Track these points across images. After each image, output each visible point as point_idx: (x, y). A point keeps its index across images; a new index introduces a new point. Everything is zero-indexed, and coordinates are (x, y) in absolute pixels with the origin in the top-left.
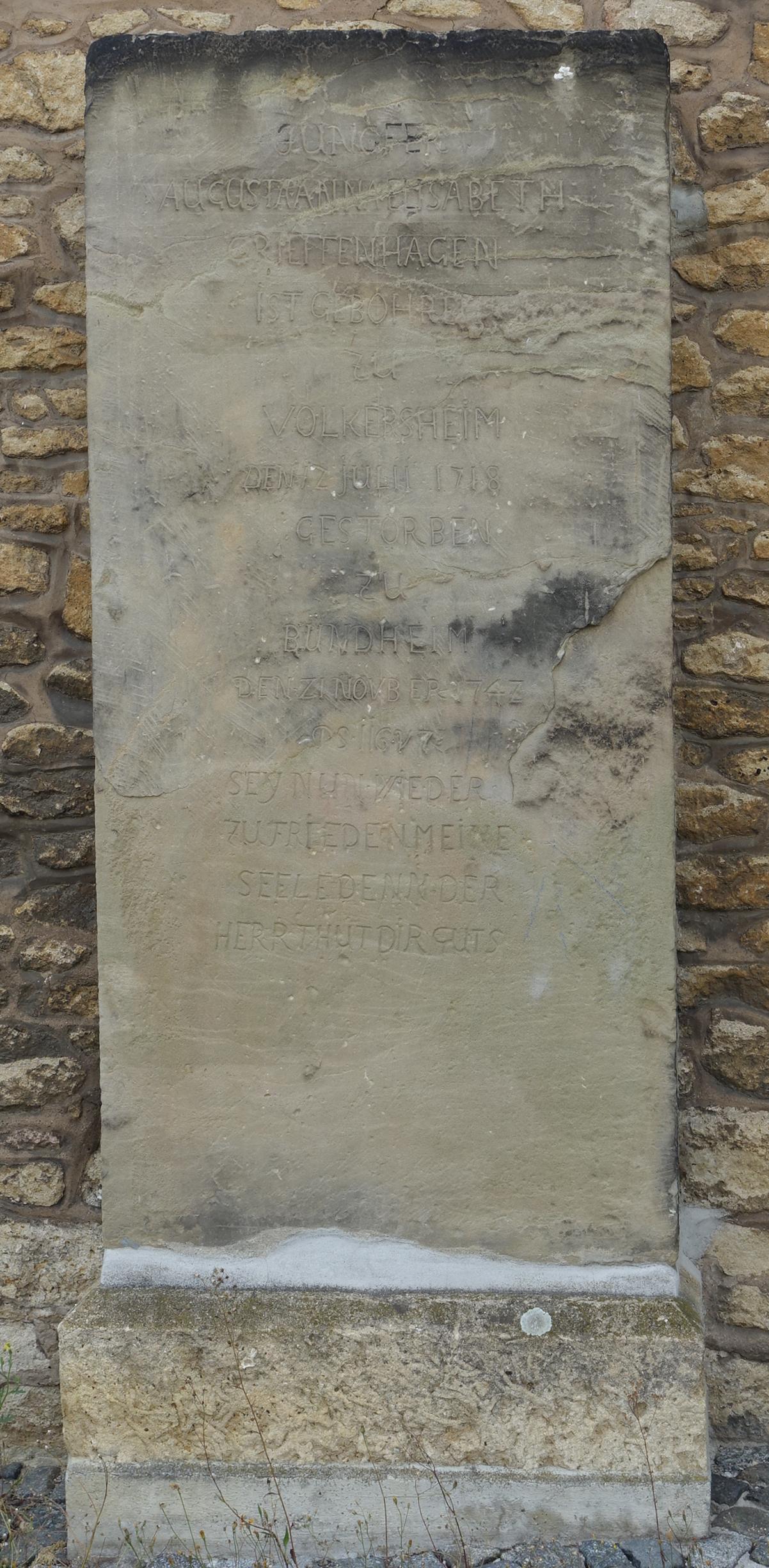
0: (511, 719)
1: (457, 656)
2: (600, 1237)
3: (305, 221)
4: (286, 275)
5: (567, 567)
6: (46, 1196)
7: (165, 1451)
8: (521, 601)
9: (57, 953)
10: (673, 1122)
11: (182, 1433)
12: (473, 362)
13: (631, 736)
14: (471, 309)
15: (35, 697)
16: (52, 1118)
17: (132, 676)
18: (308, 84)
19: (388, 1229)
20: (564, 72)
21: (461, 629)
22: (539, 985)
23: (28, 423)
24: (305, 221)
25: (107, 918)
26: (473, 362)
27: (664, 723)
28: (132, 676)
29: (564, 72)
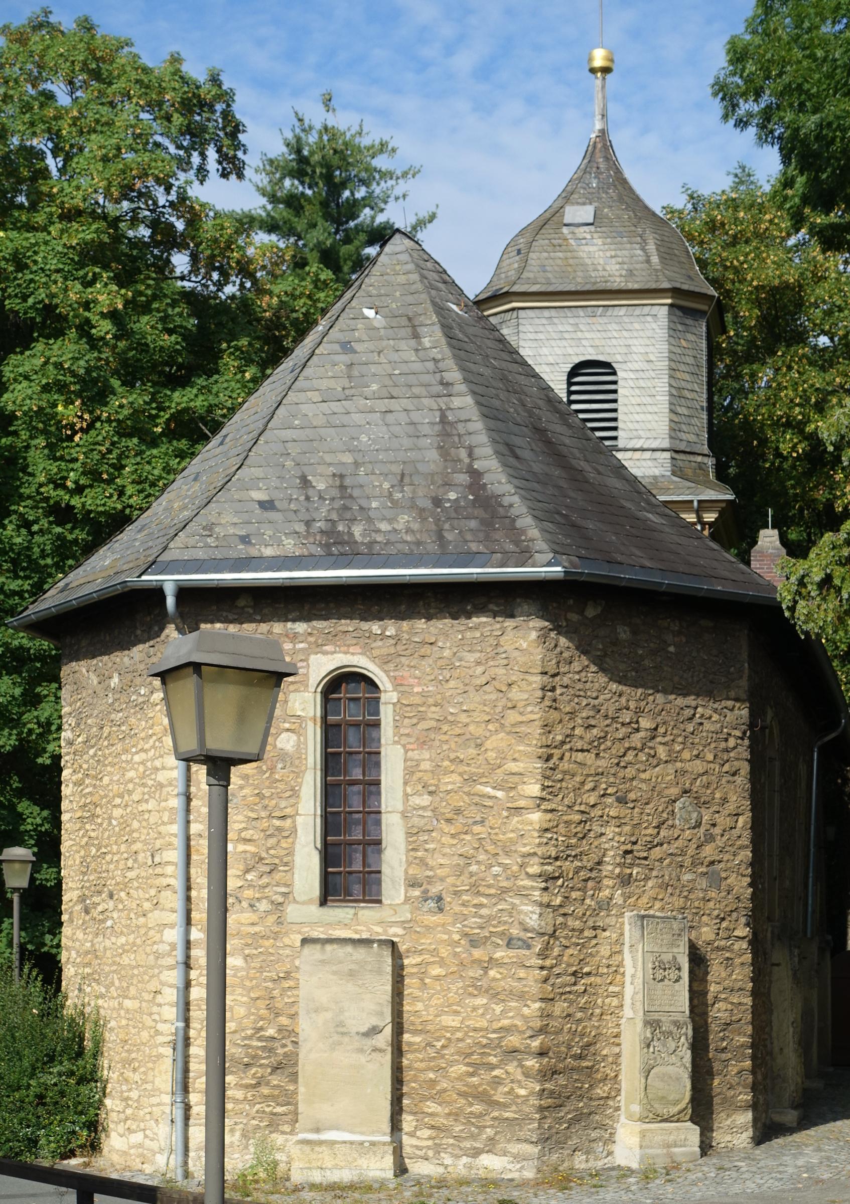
0: (365, 1048)
1: (357, 1038)
2: (378, 1132)
3: (334, 968)
4: (331, 977)
5: (375, 1024)
6: (288, 1130)
7: (307, 1165)
8: (175, 1009)
9: (292, 1088)
10: (230, 798)
11: (310, 1163)
12: (360, 991)
13: (384, 1051)
14: (360, 982)
15: (289, 1044)
16: (290, 1116)
17: (305, 1040)
18: (335, 946)
19: (344, 1130)
20: (375, 945)
21: (358, 1033)
22: (369, 1091)
23: (289, 997)
24: (334, 968)
25: (300, 1080)
26: (360, 991)
27: (390, 1049)
28: (305, 1040)
29: (375, 945)
